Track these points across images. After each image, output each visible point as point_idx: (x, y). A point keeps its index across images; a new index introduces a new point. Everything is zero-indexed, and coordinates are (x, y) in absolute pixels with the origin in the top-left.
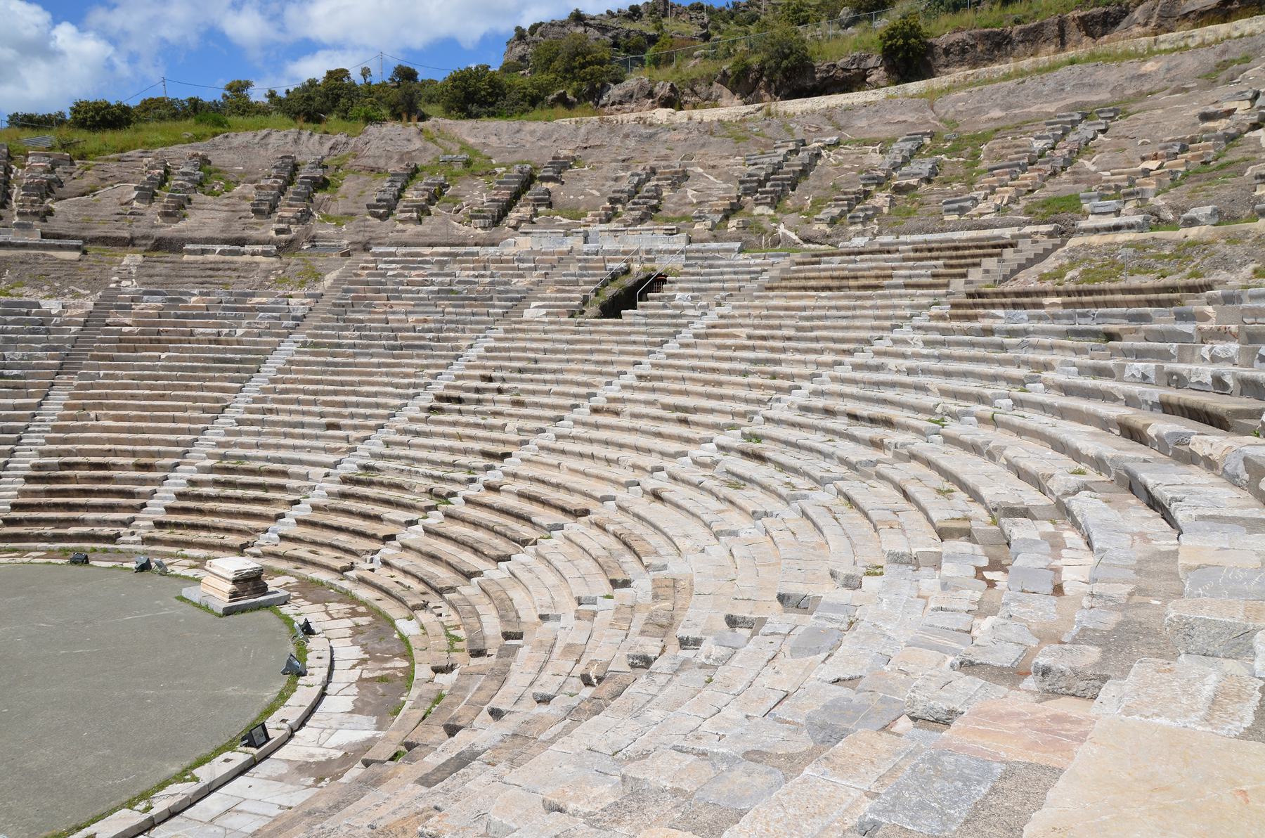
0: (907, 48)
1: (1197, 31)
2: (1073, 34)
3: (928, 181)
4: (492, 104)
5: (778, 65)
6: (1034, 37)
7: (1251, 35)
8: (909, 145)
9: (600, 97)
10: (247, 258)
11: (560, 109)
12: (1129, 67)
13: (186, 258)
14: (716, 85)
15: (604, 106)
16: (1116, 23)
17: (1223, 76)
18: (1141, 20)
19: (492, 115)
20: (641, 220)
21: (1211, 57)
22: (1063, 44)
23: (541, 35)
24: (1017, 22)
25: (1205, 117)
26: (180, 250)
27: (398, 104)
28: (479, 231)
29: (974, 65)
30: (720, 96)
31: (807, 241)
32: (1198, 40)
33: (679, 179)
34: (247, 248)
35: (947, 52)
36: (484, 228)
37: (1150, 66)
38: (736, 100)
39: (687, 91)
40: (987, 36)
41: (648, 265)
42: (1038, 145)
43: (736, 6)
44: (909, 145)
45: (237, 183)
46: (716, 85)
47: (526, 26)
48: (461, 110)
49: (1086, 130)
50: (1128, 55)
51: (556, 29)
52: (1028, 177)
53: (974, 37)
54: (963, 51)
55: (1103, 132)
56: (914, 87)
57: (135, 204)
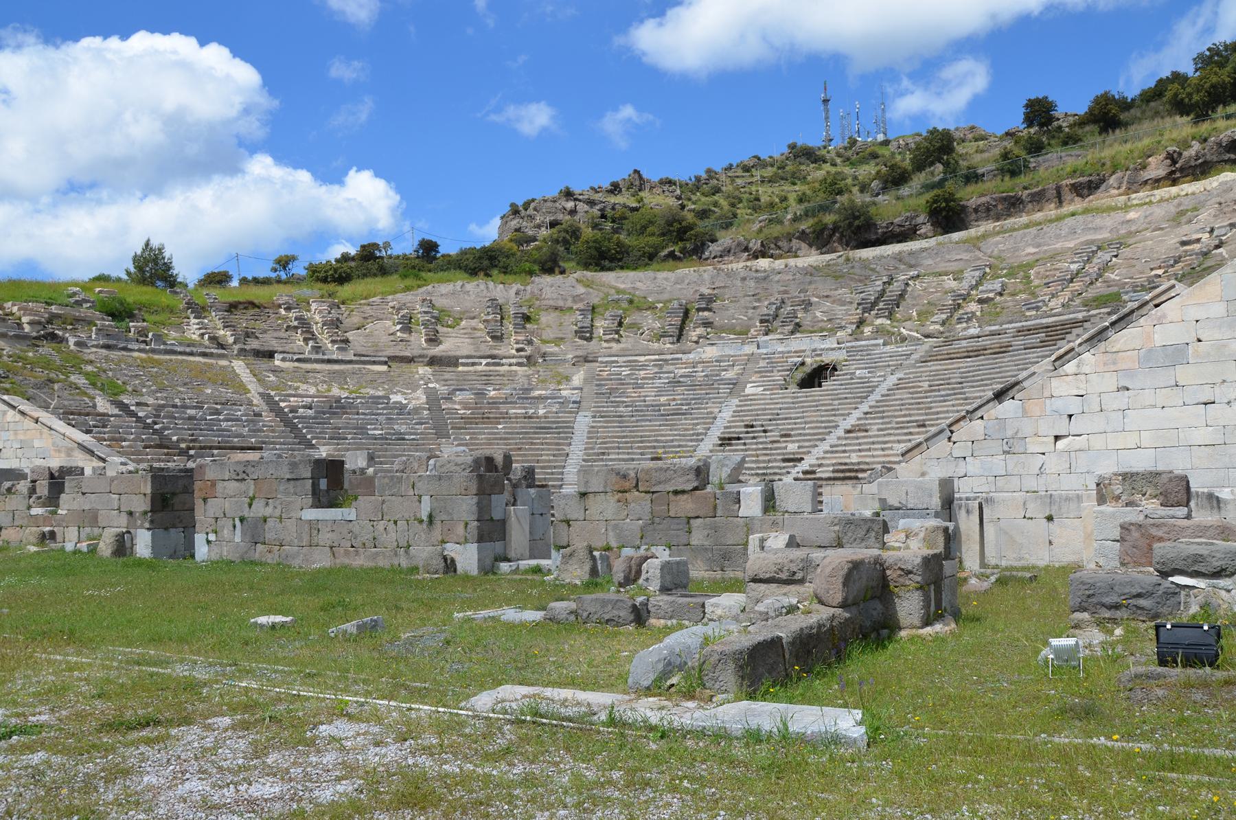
0: (949, 209)
1: (1156, 192)
2: (1067, 195)
3: (1001, 294)
4: (620, 260)
5: (850, 225)
6: (1039, 198)
7: (1193, 194)
8: (977, 273)
9: (703, 252)
10: (506, 368)
11: (671, 262)
12: (1119, 216)
13: (460, 368)
14: (794, 241)
15: (706, 259)
16: (1097, 187)
17: (1184, 219)
18: (1115, 185)
19: (622, 268)
20: (792, 333)
21: (1172, 208)
22: (1060, 203)
23: (535, 209)
24: (1025, 188)
25: (1184, 243)
26: (456, 365)
27: (546, 262)
28: (668, 346)
29: (998, 219)
30: (799, 249)
31: (927, 336)
32: (1158, 197)
33: (807, 305)
34: (504, 361)
35: (976, 210)
36: (673, 343)
37: (1132, 215)
38: (813, 251)
39: (772, 246)
40: (1005, 199)
41: (818, 359)
42: (1074, 267)
43: (698, 179)
44: (977, 273)
45: (461, 319)
46: (794, 241)
47: (520, 203)
48: (597, 265)
49: (1103, 256)
50: (1115, 209)
51: (549, 204)
52: (1076, 286)
53: (995, 200)
54: (988, 210)
55: (1116, 256)
56: (956, 236)
57: (399, 334)
